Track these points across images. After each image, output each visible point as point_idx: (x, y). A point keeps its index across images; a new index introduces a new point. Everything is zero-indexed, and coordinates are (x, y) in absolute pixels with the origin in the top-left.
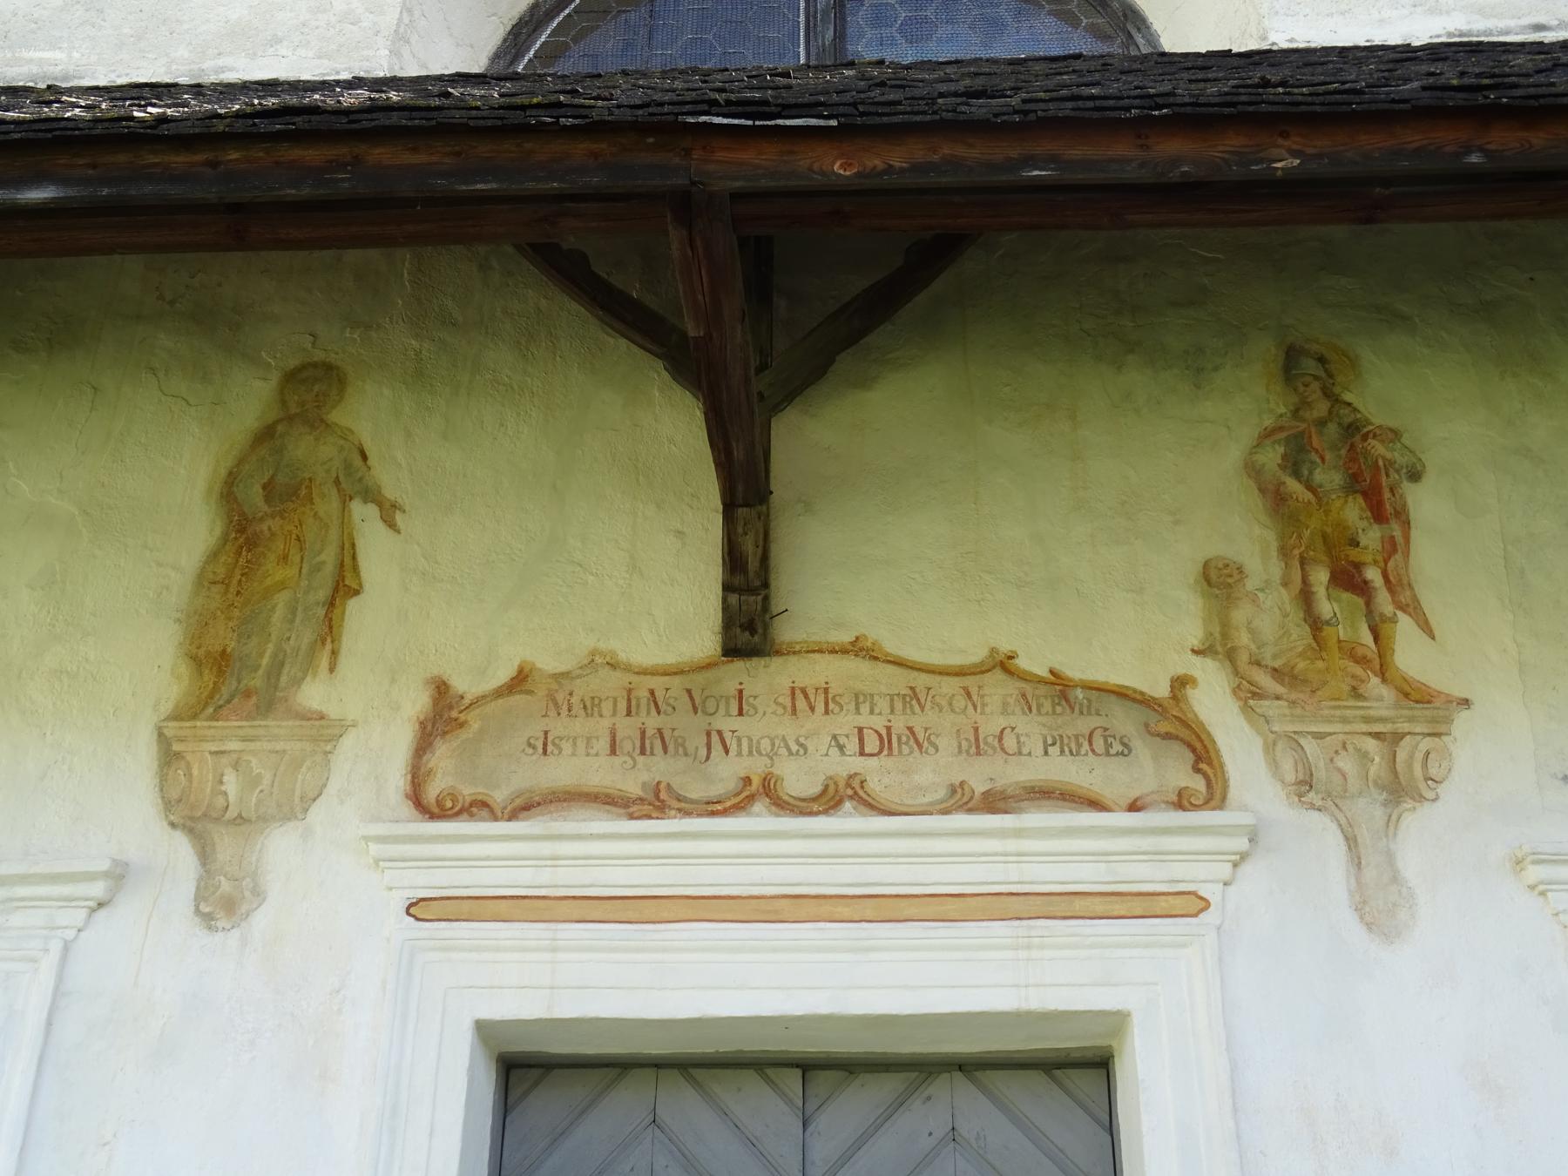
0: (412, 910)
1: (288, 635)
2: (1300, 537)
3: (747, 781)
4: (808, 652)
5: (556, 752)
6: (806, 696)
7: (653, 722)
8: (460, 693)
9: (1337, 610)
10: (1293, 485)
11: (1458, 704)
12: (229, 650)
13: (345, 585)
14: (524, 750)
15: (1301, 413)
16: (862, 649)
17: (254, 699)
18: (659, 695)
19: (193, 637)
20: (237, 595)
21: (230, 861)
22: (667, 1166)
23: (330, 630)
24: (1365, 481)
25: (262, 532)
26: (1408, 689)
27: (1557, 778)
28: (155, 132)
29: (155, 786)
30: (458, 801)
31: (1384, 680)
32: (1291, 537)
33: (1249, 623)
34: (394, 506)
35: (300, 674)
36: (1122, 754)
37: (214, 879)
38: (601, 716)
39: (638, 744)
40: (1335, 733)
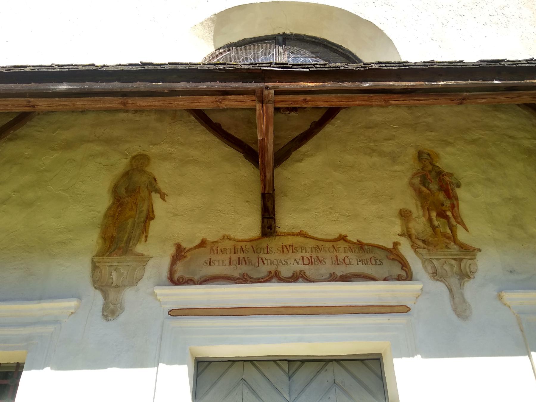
0: (408, 309)
1: (132, 231)
2: (427, 203)
3: (270, 272)
4: (287, 235)
5: (213, 264)
6: (287, 248)
7: (242, 255)
8: (185, 247)
9: (439, 223)
10: (424, 189)
11: (477, 250)
12: (114, 235)
14: (204, 264)
15: (424, 169)
16: (302, 234)
17: (122, 250)
18: (244, 247)
19: (103, 232)
20: (117, 220)
21: (113, 299)
22: (247, 393)
24: (444, 187)
25: (125, 201)
26: (462, 246)
27: (508, 271)
28: (101, 69)
29: (90, 276)
30: (184, 279)
31: (455, 244)
32: (424, 203)
33: (414, 227)
34: (165, 194)
35: (136, 243)
36: (380, 264)
37: (108, 304)
38: (227, 254)
39: (238, 262)
40: (442, 259)
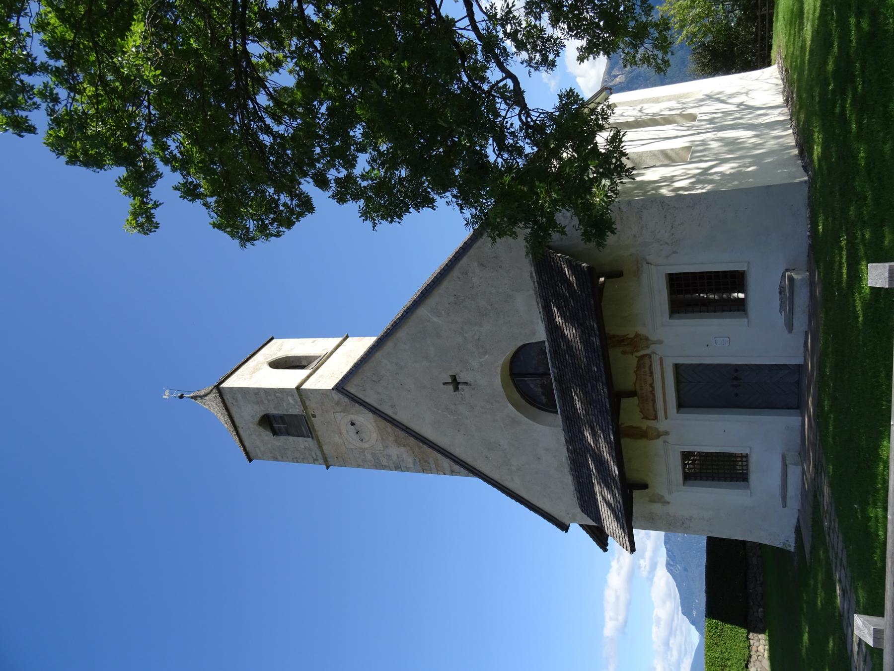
13: (632, 427)
23: (637, 428)
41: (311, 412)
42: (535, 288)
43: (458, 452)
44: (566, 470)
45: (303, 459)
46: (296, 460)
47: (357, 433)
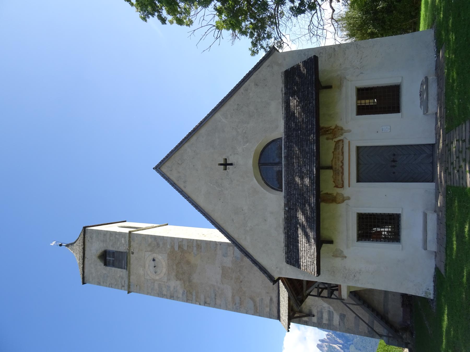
13: (327, 194)
23: (330, 194)
41: (132, 250)
42: (283, 97)
43: (215, 216)
44: (281, 230)
45: (116, 285)
46: (111, 286)
47: (155, 267)
